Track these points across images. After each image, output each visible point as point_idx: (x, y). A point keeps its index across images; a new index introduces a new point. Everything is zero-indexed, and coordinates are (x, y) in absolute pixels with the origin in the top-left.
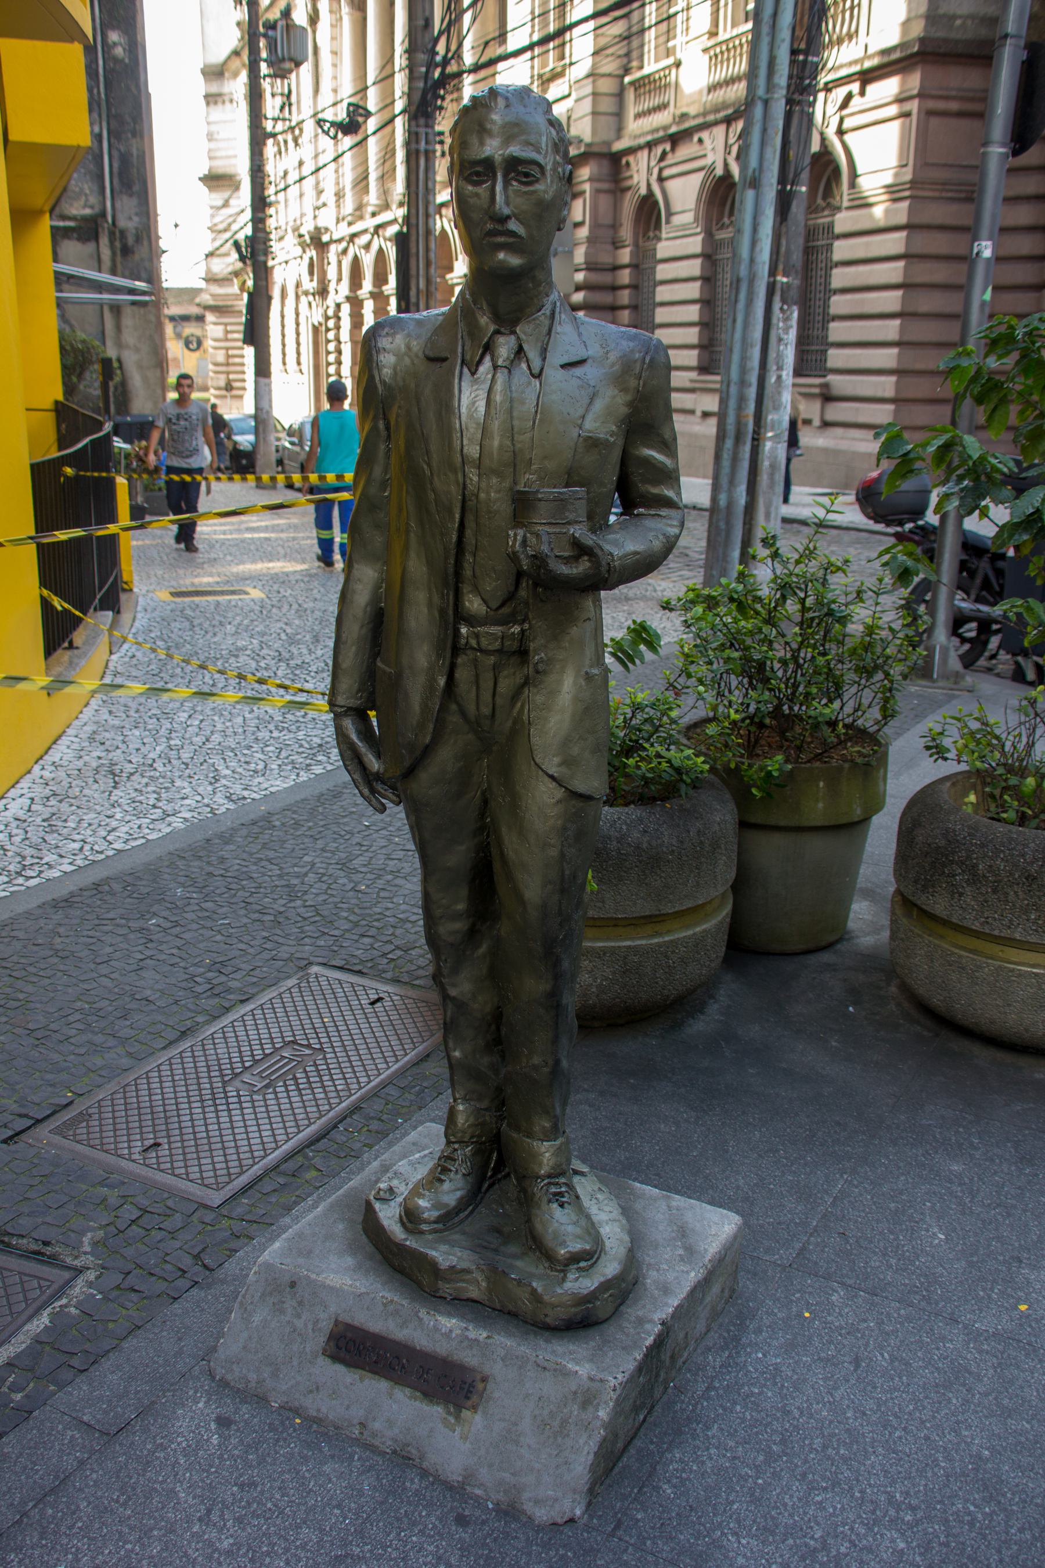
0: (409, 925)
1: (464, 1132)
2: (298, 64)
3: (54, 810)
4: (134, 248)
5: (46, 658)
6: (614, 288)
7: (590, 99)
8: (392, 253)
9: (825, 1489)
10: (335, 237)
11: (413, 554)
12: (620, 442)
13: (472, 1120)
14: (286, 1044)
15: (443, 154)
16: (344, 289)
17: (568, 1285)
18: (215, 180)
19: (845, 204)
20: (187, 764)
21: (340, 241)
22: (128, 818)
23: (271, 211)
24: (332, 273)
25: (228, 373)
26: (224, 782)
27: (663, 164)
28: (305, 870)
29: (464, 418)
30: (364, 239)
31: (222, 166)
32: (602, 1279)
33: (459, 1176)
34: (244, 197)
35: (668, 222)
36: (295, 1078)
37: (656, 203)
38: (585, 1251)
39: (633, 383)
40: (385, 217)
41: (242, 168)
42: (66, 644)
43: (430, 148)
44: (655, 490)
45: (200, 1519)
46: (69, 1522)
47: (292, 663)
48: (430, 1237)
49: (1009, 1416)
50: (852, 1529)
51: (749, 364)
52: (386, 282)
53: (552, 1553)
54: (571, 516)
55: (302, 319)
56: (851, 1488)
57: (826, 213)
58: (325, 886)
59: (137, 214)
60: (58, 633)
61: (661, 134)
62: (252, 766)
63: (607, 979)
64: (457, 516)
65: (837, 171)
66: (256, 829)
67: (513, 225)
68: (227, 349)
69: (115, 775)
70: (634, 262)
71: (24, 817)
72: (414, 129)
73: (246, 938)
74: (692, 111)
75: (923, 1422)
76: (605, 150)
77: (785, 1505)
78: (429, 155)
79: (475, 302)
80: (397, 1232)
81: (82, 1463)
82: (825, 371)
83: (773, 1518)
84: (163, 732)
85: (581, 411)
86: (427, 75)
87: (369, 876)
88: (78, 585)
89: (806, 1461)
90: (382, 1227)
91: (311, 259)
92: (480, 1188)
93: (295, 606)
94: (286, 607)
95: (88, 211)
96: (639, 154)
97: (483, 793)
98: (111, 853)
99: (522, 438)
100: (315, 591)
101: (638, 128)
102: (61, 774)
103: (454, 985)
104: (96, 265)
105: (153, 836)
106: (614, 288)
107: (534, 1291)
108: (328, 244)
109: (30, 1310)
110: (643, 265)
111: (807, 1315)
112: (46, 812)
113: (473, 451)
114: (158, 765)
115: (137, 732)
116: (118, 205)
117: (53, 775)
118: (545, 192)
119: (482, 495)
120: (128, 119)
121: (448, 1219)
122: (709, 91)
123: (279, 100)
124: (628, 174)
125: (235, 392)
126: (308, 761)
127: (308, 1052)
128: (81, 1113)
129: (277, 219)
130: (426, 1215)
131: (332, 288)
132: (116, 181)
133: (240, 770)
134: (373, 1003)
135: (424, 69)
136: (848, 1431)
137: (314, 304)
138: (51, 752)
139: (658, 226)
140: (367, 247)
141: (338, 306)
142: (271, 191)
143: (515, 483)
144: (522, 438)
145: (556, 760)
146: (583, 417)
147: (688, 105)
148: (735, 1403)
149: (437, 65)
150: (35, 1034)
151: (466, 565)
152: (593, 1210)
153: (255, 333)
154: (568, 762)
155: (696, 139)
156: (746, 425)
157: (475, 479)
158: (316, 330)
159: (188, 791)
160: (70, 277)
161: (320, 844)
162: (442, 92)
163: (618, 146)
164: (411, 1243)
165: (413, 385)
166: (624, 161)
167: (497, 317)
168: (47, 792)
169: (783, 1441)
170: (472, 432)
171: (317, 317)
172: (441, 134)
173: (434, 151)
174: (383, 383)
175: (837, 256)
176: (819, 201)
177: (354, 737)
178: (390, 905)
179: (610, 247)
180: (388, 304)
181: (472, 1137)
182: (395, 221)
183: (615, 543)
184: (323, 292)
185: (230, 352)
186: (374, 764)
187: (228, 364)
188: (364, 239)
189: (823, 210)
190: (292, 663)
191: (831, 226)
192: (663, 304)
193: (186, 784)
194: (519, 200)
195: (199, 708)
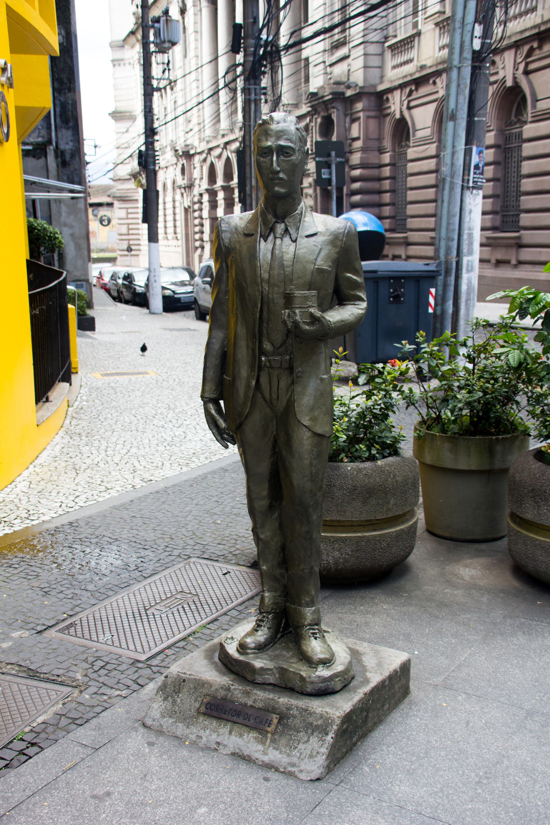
0: (244, 539)
1: (268, 607)
2: (174, 44)
3: (43, 487)
4: (71, 164)
5: (37, 403)
6: (380, 179)
7: (363, 57)
8: (234, 159)
9: (445, 770)
10: (199, 150)
11: (239, 324)
12: (334, 270)
13: (272, 601)
14: (178, 592)
15: (266, 102)
16: (205, 185)
17: (317, 673)
18: (118, 116)
19: (530, 119)
20: (117, 464)
21: (200, 153)
22: (85, 491)
23: (156, 138)
24: (196, 174)
25: (129, 240)
26: (139, 472)
27: (410, 98)
28: (186, 514)
29: (261, 261)
30: (217, 152)
31: (123, 106)
32: (335, 671)
33: (266, 628)
34: (140, 124)
35: (414, 136)
36: (183, 607)
37: (406, 123)
38: (326, 658)
39: (339, 243)
40: (231, 137)
41: (137, 106)
42: (44, 399)
43: (258, 98)
44: (352, 293)
45: (141, 779)
46: (79, 780)
47: (177, 411)
48: (251, 656)
49: (543, 746)
50: (456, 785)
51: (452, 227)
52: (232, 179)
53: (309, 791)
54: (310, 303)
55: (177, 204)
56: (458, 770)
57: (517, 126)
58: (198, 521)
59: (71, 141)
60: (42, 393)
61: (409, 78)
62: (155, 465)
63: (348, 554)
64: (259, 306)
65: (524, 98)
66: (158, 495)
67: (281, 175)
68: (129, 224)
69: (76, 470)
70: (393, 162)
71: (26, 491)
72: (247, 87)
73: (155, 546)
74: (429, 63)
75: (498, 746)
76: (372, 90)
77: (424, 776)
78: (257, 102)
79: (266, 209)
80: (236, 655)
81: (83, 759)
82: (519, 228)
83: (417, 780)
84: (103, 447)
85: (315, 257)
86: (255, 53)
87: (222, 516)
88: (52, 365)
89: (437, 760)
90: (228, 653)
91: (183, 165)
92: (276, 637)
93: (177, 380)
94: (171, 381)
95: (40, 139)
96: (395, 92)
97: (274, 437)
98: (77, 508)
99: (288, 269)
100: (189, 372)
101: (394, 75)
102: (45, 469)
103: (262, 533)
104: (46, 173)
105: (101, 499)
106: (380, 179)
107: (301, 676)
108: (193, 155)
109: (53, 703)
110: (399, 163)
111: (444, 704)
112: (39, 488)
113: (265, 276)
114: (101, 464)
115: (87, 448)
116: (60, 135)
117: (41, 470)
118: (296, 160)
119: (270, 296)
120: (65, 81)
121: (261, 648)
122: (440, 50)
123: (161, 68)
124: (388, 105)
125: (133, 253)
126: (187, 462)
127: (190, 596)
128: (71, 623)
129: (162, 141)
130: (250, 646)
131: (197, 182)
132: (58, 120)
133: (148, 466)
134: (225, 574)
135: (252, 49)
136: (459, 749)
137: (185, 195)
138: (38, 458)
139: (408, 139)
140: (219, 157)
141: (201, 195)
142: (156, 125)
143: (285, 290)
144: (288, 269)
145: (307, 418)
146: (316, 259)
147: (426, 60)
148: (403, 738)
149: (261, 47)
150: (44, 590)
151: (264, 328)
152: (333, 646)
153: (150, 215)
154: (314, 419)
155: (431, 81)
156: (451, 264)
157: (267, 288)
158: (186, 210)
159: (119, 477)
160: (34, 183)
161: (195, 502)
162: (265, 63)
163: (381, 88)
164: (241, 658)
165: (238, 247)
166: (385, 97)
167: (276, 216)
168: (38, 479)
169: (426, 753)
170: (266, 267)
171: (187, 203)
172: (265, 88)
173: (260, 100)
174: (225, 246)
175: (525, 153)
176: (513, 118)
177: (213, 412)
178: (234, 530)
179: (376, 153)
180: (233, 193)
181: (272, 609)
182: (236, 140)
183: (331, 317)
184: (190, 187)
185: (131, 227)
186: (222, 424)
187: (128, 234)
188: (217, 152)
189: (515, 123)
190: (177, 411)
191: (521, 133)
192: (412, 189)
193: (118, 474)
194: (283, 164)
195: (123, 435)
